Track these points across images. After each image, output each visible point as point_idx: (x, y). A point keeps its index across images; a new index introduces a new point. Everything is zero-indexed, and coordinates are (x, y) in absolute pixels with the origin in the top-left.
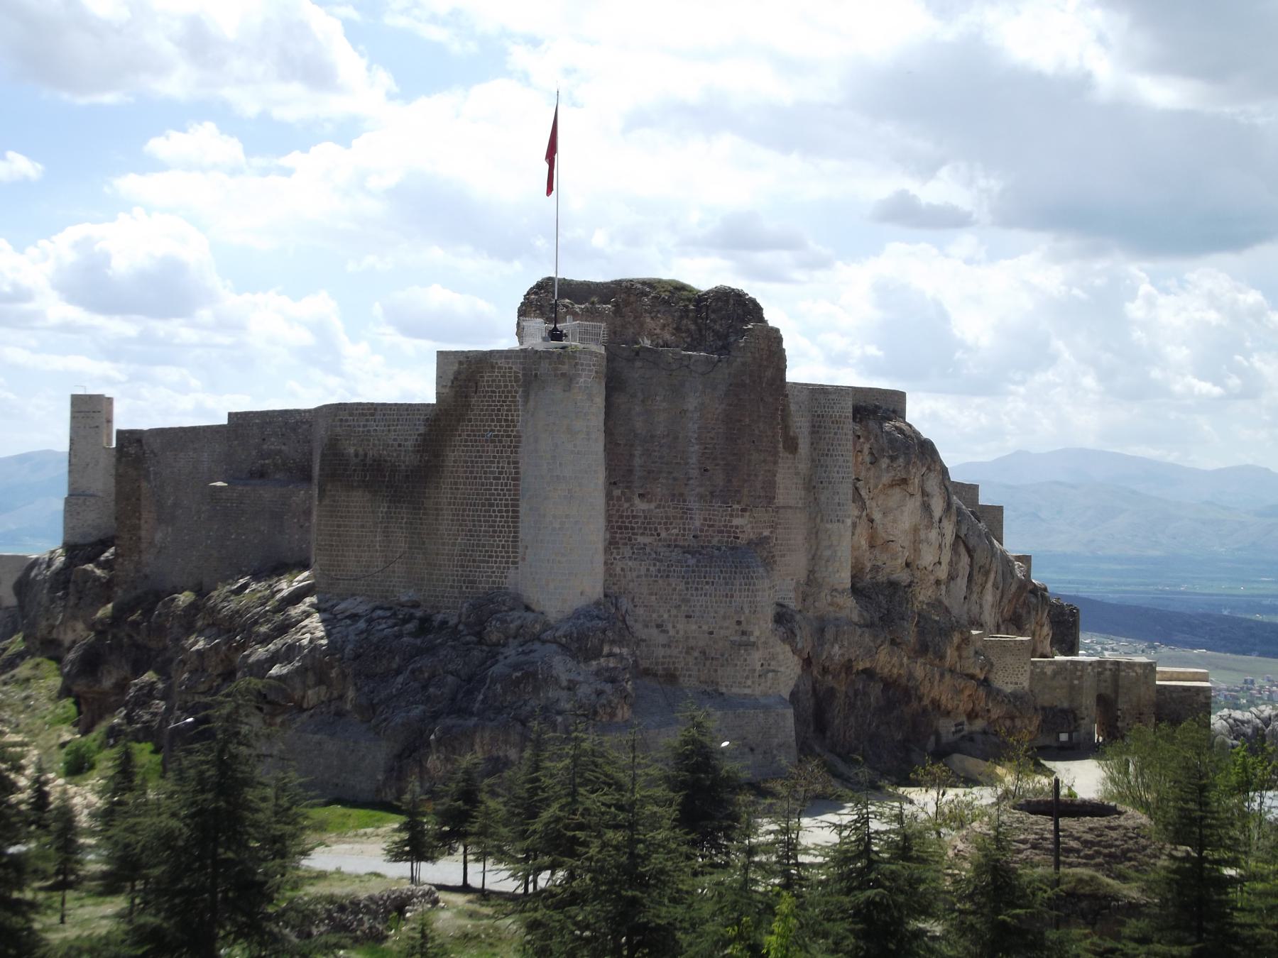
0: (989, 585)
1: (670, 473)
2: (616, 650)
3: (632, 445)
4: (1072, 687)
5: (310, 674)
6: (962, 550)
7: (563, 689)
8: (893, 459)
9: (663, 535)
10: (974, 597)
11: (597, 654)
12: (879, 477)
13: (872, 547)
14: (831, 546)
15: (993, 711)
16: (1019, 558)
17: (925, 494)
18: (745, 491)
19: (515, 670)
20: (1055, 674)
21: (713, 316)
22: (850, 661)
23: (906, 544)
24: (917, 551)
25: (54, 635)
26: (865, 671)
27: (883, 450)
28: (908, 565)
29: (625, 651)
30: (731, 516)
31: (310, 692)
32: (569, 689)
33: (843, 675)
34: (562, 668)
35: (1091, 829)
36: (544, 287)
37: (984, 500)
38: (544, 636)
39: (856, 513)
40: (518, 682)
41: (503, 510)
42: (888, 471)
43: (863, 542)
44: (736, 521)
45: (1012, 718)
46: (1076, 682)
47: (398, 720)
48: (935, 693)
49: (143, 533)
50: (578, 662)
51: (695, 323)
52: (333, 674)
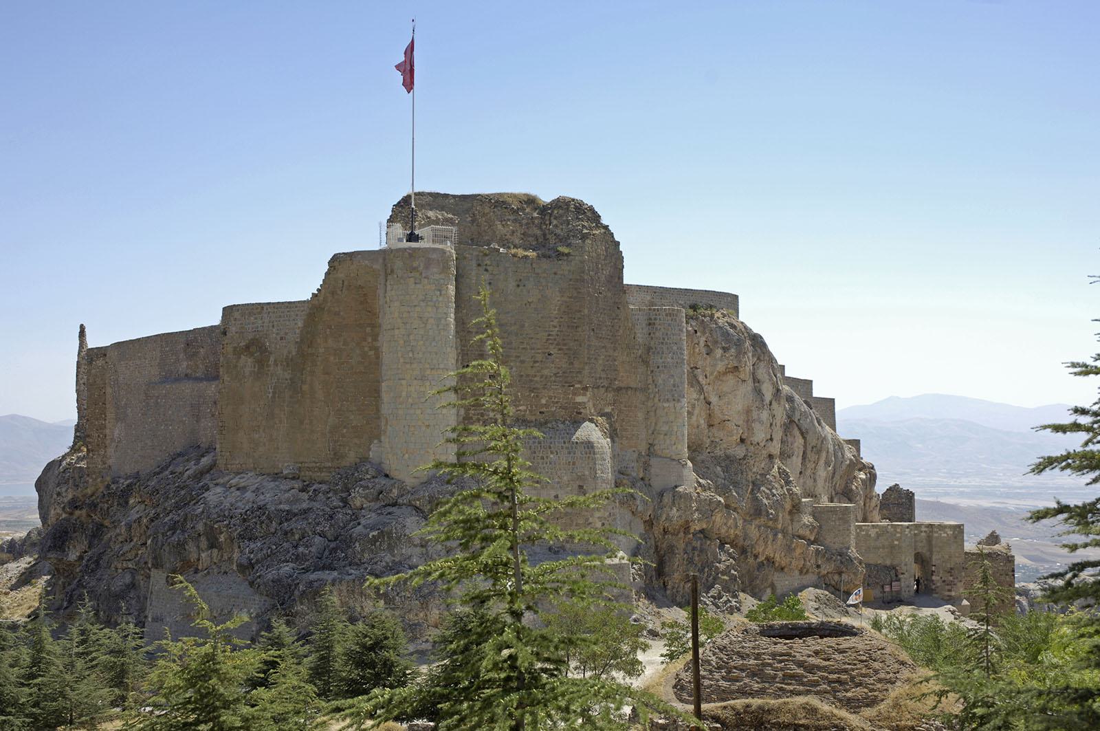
0: (822, 462)
4: (892, 547)
5: (203, 539)
6: (796, 432)
7: (415, 546)
8: (725, 349)
10: (809, 472)
12: (714, 366)
13: (711, 426)
15: (823, 567)
16: (849, 442)
17: (756, 380)
18: (586, 372)
19: (372, 529)
20: (878, 536)
21: (555, 222)
22: (687, 522)
24: (750, 429)
26: (702, 531)
27: (716, 342)
28: (742, 440)
30: (575, 394)
31: (203, 555)
32: (422, 546)
33: (682, 534)
35: (817, 653)
36: (406, 201)
37: (817, 392)
38: (400, 501)
39: (695, 396)
40: (375, 539)
42: (721, 360)
43: (702, 422)
44: (579, 399)
45: (840, 573)
46: (896, 543)
47: (270, 576)
48: (769, 552)
51: (540, 228)
52: (222, 538)
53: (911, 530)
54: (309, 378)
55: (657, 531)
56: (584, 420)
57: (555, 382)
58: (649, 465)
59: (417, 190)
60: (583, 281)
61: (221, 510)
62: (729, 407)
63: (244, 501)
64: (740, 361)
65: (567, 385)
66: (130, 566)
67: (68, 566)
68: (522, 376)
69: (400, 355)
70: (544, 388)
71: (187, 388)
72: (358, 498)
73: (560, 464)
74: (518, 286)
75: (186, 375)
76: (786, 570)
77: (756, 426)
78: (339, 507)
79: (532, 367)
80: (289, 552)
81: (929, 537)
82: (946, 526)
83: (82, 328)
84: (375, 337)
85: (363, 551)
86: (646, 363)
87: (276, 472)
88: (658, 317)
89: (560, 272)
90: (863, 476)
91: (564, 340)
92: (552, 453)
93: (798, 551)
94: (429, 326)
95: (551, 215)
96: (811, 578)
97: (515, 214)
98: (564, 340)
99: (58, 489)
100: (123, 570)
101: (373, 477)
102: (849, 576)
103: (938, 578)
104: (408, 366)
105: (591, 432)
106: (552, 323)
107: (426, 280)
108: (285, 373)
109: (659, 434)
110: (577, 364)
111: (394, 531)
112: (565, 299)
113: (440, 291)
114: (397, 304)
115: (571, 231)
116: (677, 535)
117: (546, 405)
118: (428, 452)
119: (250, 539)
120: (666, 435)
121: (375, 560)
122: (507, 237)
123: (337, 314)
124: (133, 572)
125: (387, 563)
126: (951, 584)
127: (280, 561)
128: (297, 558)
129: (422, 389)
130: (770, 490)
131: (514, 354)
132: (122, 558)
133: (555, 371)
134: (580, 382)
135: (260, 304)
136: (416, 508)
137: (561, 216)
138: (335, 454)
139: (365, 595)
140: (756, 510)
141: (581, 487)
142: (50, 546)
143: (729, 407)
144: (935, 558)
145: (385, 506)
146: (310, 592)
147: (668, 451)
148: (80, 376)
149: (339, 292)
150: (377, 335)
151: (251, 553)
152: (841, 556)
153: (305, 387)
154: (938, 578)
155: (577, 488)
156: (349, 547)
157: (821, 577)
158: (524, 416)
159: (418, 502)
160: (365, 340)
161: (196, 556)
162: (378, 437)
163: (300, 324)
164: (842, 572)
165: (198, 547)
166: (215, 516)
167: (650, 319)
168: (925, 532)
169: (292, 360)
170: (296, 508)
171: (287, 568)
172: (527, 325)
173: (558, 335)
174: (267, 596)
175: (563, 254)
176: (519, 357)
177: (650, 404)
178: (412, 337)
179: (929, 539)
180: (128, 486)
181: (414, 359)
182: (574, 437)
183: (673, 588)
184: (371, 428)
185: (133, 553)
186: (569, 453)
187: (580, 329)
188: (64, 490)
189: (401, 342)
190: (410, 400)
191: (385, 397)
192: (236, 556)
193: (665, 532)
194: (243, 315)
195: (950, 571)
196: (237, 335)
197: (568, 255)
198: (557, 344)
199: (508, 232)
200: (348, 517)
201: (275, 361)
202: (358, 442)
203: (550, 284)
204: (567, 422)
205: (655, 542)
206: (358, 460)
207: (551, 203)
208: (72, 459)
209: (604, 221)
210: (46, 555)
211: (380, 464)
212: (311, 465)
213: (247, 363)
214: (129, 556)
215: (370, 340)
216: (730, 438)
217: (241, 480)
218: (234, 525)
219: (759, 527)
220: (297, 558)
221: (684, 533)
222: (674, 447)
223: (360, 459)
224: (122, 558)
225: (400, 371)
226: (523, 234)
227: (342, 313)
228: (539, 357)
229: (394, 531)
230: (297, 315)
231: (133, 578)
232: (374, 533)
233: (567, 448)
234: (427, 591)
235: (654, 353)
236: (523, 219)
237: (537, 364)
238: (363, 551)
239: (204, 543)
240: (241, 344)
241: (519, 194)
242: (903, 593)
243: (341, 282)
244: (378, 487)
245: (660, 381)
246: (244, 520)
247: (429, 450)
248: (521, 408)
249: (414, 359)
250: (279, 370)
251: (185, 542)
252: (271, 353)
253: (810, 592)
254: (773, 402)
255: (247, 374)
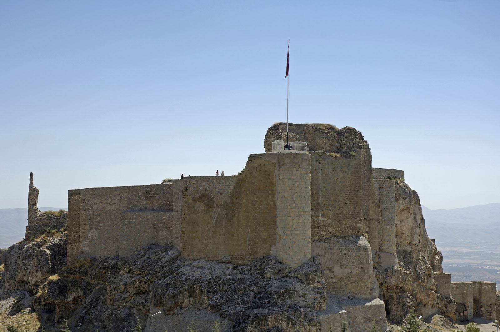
1: (333, 205)
2: (320, 280)
3: (318, 193)
4: (463, 294)
5: (186, 292)
8: (404, 199)
9: (331, 231)
11: (313, 281)
12: (399, 207)
14: (388, 236)
17: (415, 214)
20: (457, 288)
21: (346, 139)
23: (409, 234)
24: (413, 237)
25: (25, 279)
27: (400, 195)
28: (410, 243)
29: (323, 280)
30: (356, 223)
31: (186, 300)
34: (299, 287)
38: (290, 275)
41: (268, 219)
42: (402, 204)
44: (358, 225)
45: (446, 307)
46: (465, 292)
49: (81, 234)
50: (305, 285)
51: (339, 142)
53: (472, 286)
54: (236, 214)
55: (384, 288)
56: (360, 235)
57: (348, 217)
58: (380, 256)
59: (290, 122)
60: (360, 169)
61: (196, 278)
62: (405, 227)
63: (205, 274)
64: (411, 204)
65: (353, 218)
66: (128, 305)
67: (65, 303)
68: (334, 214)
69: (288, 204)
70: (344, 220)
71: (150, 215)
72: (268, 274)
73: (353, 257)
74: (333, 171)
75: (146, 208)
76: (426, 306)
77: (415, 235)
78: (259, 278)
79: (339, 210)
80: (239, 299)
81: (479, 288)
82: (488, 284)
83: (31, 174)
84: (274, 195)
85: (278, 299)
86: (379, 207)
87: (217, 259)
88: (384, 185)
89: (351, 164)
90: (438, 258)
91: (352, 197)
92: (349, 251)
93: (431, 297)
94: (302, 191)
95: (343, 136)
96: (435, 310)
97: (326, 134)
98: (352, 197)
99: (23, 261)
100: (123, 307)
101: (274, 263)
102: (451, 308)
103: (484, 309)
104: (293, 210)
105: (363, 241)
106: (347, 189)
107: (301, 169)
108: (223, 211)
109: (384, 241)
110: (357, 209)
111: (292, 290)
112: (353, 177)
113: (307, 174)
114: (287, 180)
115: (353, 144)
116: (393, 290)
117: (345, 228)
118: (302, 252)
119: (213, 293)
120: (388, 241)
121: (284, 304)
122: (322, 146)
123: (253, 183)
124: (130, 308)
125: (290, 305)
126: (490, 312)
127: (235, 304)
128: (244, 302)
129: (299, 221)
130: (421, 267)
131: (332, 204)
132: (123, 301)
133: (348, 211)
134: (359, 217)
135: (208, 177)
136: (298, 278)
137: (349, 136)
138: (251, 251)
139: (283, 320)
140: (417, 277)
141: (362, 268)
142: (58, 294)
143: (405, 227)
144: (483, 299)
145: (282, 277)
146: (257, 319)
147: (388, 249)
148: (31, 200)
149: (254, 173)
150: (275, 194)
151: (217, 299)
152: (447, 299)
153: (235, 219)
154: (484, 309)
155: (360, 268)
156: (270, 297)
157: (439, 309)
158: (335, 233)
159: (299, 276)
160: (268, 197)
161: (182, 301)
162: (275, 244)
163: (232, 187)
164: (447, 307)
165: (184, 296)
166: (193, 281)
167: (380, 185)
168: (478, 286)
169: (227, 205)
170: (236, 278)
171: (239, 307)
172: (337, 189)
173: (350, 194)
174: (231, 321)
175: (352, 155)
176: (333, 205)
177: (380, 226)
178: (294, 196)
179: (480, 290)
180: (115, 264)
181: (296, 207)
182: (358, 244)
183: (393, 315)
184: (271, 239)
185: (129, 298)
186: (357, 251)
187: (359, 192)
188: (27, 262)
189: (289, 199)
190: (294, 227)
191: (279, 224)
192: (206, 301)
193: (388, 288)
194: (198, 181)
195: (490, 306)
196: (194, 191)
197: (354, 156)
198: (349, 199)
199: (323, 143)
200: (265, 282)
201: (217, 205)
202: (265, 246)
203: (347, 170)
204: (354, 236)
205: (384, 294)
206: (265, 255)
207: (343, 129)
208: (30, 245)
209: (365, 139)
210: (56, 298)
211: (276, 256)
212: (238, 257)
213: (200, 206)
214: (127, 300)
215: (271, 197)
216: (405, 242)
217: (199, 263)
218: (204, 286)
219: (418, 285)
220: (244, 302)
221: (396, 289)
222: (391, 247)
223: (266, 254)
224: (123, 301)
225: (288, 213)
226: (330, 145)
227: (256, 183)
228: (342, 205)
229: (292, 290)
230: (230, 183)
231: (130, 311)
232: (282, 291)
233: (356, 249)
234: (310, 318)
235: (382, 202)
236: (330, 137)
237: (341, 209)
238: (278, 299)
239: (187, 294)
240: (196, 196)
241: (326, 124)
242: (469, 317)
243: (255, 168)
244: (278, 268)
245: (385, 216)
246: (209, 284)
247: (302, 250)
248: (334, 229)
249: (296, 207)
250: (219, 210)
251: (178, 294)
252: (214, 201)
253: (437, 316)
254: (421, 224)
255: (200, 211)
